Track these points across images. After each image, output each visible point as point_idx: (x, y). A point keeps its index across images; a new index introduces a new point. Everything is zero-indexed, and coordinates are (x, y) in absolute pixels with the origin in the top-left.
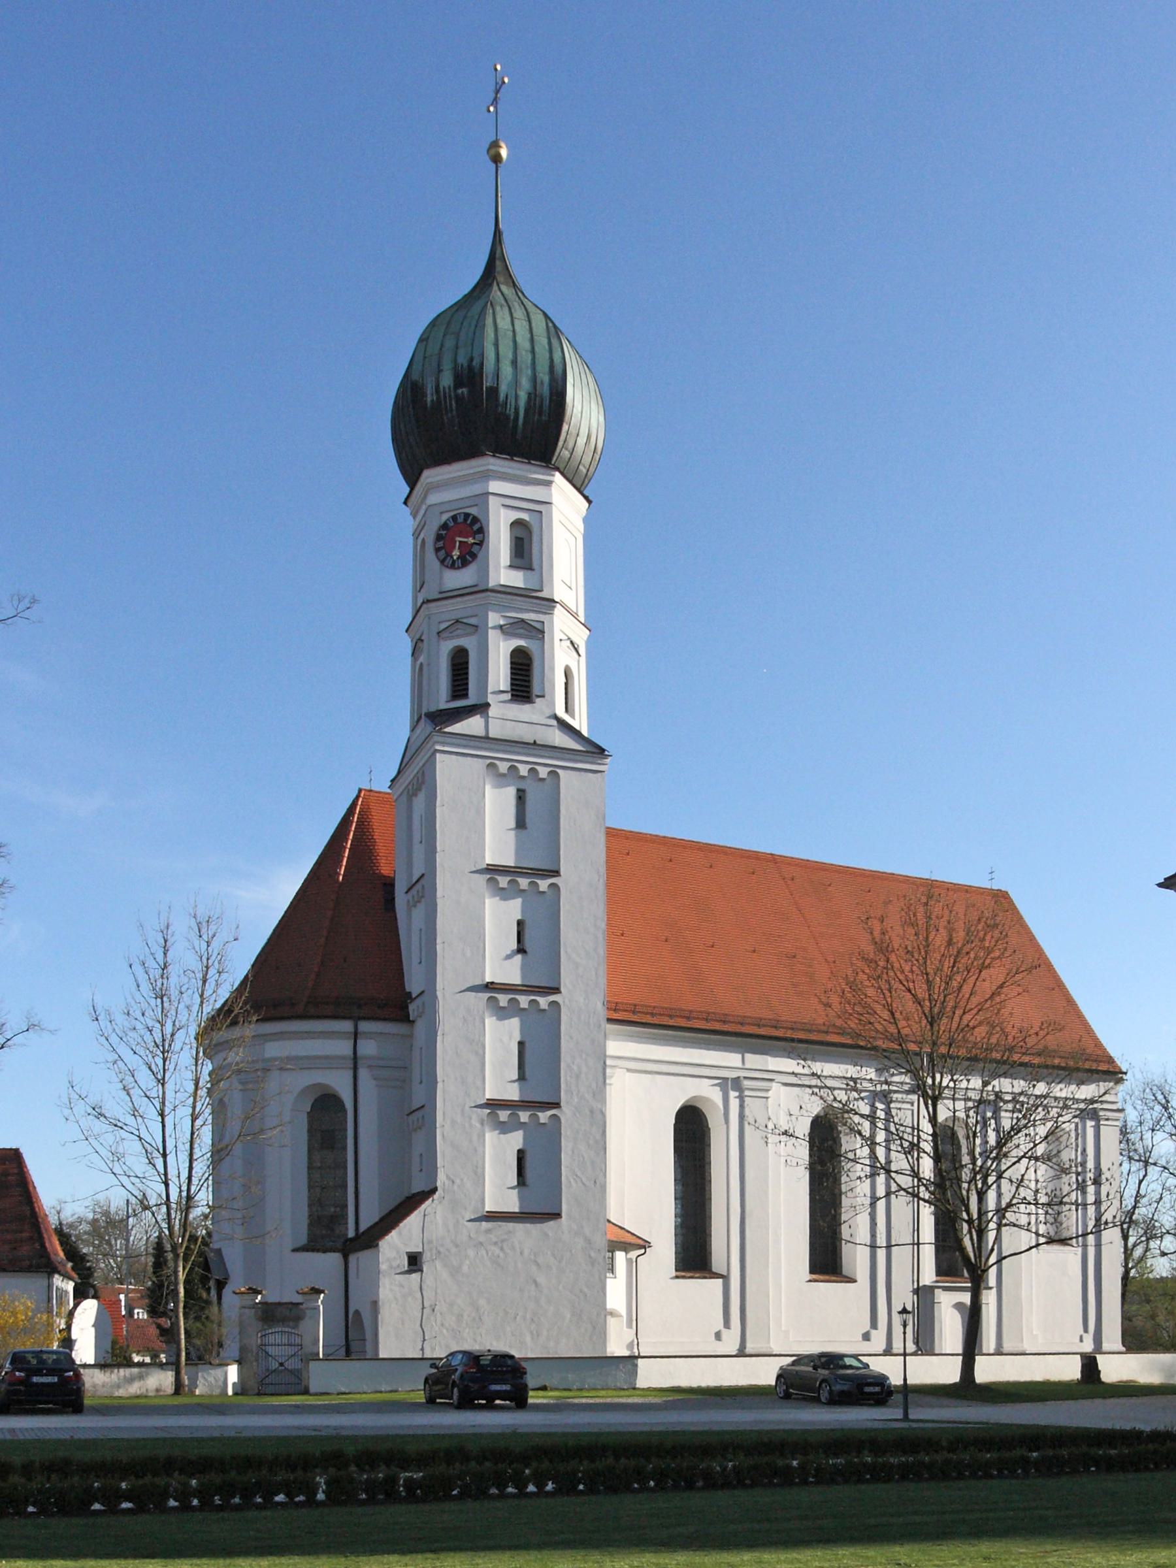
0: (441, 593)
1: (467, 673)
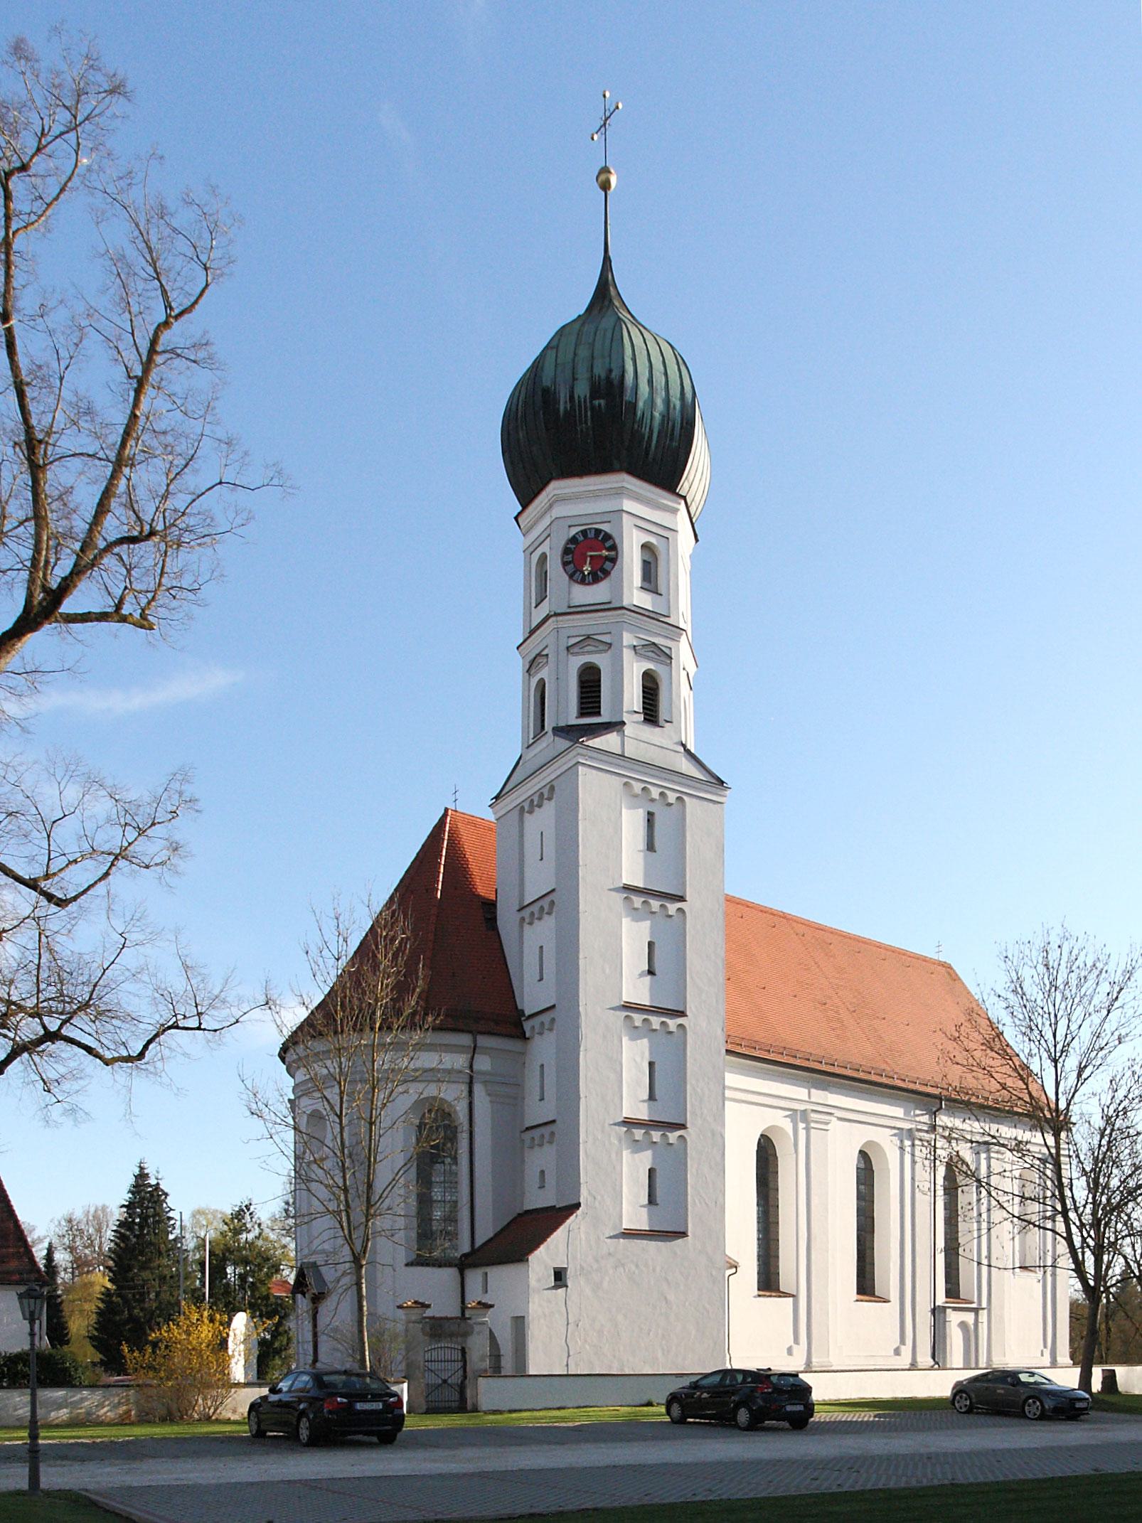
0: (569, 607)
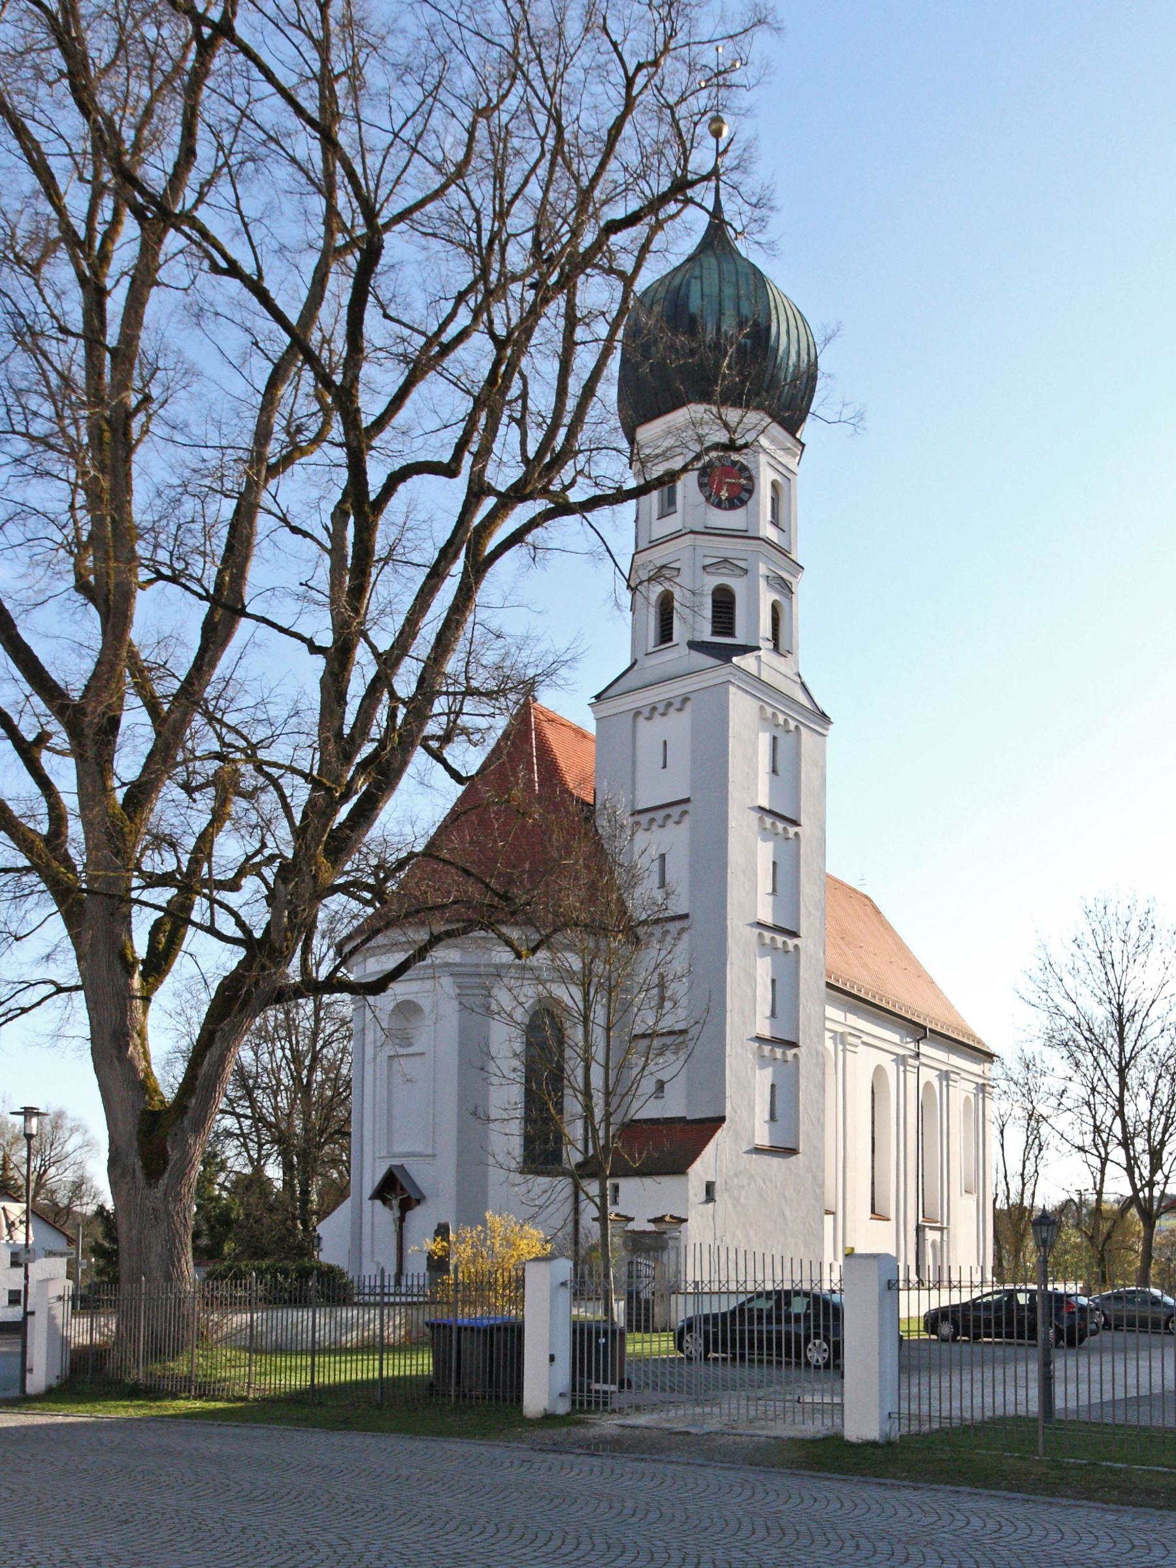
1: (671, 628)
